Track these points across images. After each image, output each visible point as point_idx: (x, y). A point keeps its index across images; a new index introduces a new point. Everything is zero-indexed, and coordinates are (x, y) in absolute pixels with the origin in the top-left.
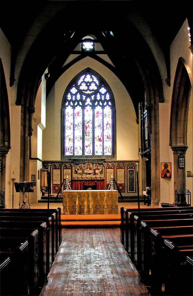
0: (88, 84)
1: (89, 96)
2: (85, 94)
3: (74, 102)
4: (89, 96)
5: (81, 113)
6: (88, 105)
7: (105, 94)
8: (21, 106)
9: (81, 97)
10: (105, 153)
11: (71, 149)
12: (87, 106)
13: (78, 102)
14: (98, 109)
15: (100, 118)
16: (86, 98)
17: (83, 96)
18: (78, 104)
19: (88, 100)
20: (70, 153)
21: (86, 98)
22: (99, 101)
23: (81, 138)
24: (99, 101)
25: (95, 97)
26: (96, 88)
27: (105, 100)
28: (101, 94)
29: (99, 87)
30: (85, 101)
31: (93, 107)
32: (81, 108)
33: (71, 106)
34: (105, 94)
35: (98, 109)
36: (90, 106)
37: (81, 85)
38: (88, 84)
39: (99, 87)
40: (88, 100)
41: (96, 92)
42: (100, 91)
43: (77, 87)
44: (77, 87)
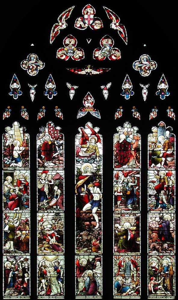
0: (88, 40)
1: (90, 85)
2: (76, 80)
3: (33, 109)
4: (90, 85)
5: (61, 151)
6: (89, 118)
7: (153, 80)
8: (91, 206)
9: (62, 91)
10: (150, 292)
11: (23, 277)
12: (82, 122)
13: (50, 106)
14: (126, 133)
15: (133, 165)
16: (80, 96)
17: (69, 85)
18: (50, 116)
19: (89, 102)
20: (20, 293)
21: (80, 96)
22: (50, 106)
23: (139, 277)
24: (127, 106)
25: (116, 91)
26: (117, 55)
27: (154, 100)
28: (137, 79)
29: (131, 53)
30: (78, 104)
31: (107, 130)
32: (8, 128)
33: (23, 123)
34: (153, 80)
35: (126, 133)
36: (95, 122)
37: (59, 43)
38: (88, 40)
39: (131, 53)
40: (89, 102)
41: (116, 71)
42: (136, 65)
43: (47, 53)
44: (47, 53)
